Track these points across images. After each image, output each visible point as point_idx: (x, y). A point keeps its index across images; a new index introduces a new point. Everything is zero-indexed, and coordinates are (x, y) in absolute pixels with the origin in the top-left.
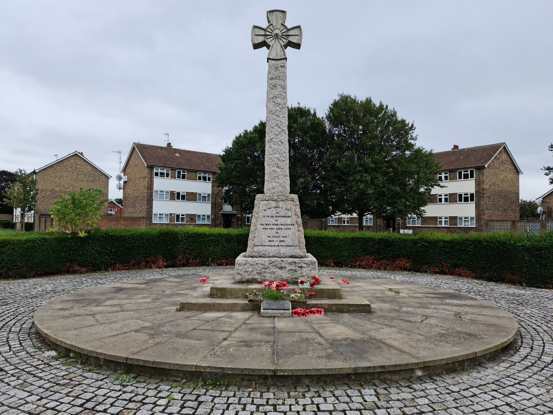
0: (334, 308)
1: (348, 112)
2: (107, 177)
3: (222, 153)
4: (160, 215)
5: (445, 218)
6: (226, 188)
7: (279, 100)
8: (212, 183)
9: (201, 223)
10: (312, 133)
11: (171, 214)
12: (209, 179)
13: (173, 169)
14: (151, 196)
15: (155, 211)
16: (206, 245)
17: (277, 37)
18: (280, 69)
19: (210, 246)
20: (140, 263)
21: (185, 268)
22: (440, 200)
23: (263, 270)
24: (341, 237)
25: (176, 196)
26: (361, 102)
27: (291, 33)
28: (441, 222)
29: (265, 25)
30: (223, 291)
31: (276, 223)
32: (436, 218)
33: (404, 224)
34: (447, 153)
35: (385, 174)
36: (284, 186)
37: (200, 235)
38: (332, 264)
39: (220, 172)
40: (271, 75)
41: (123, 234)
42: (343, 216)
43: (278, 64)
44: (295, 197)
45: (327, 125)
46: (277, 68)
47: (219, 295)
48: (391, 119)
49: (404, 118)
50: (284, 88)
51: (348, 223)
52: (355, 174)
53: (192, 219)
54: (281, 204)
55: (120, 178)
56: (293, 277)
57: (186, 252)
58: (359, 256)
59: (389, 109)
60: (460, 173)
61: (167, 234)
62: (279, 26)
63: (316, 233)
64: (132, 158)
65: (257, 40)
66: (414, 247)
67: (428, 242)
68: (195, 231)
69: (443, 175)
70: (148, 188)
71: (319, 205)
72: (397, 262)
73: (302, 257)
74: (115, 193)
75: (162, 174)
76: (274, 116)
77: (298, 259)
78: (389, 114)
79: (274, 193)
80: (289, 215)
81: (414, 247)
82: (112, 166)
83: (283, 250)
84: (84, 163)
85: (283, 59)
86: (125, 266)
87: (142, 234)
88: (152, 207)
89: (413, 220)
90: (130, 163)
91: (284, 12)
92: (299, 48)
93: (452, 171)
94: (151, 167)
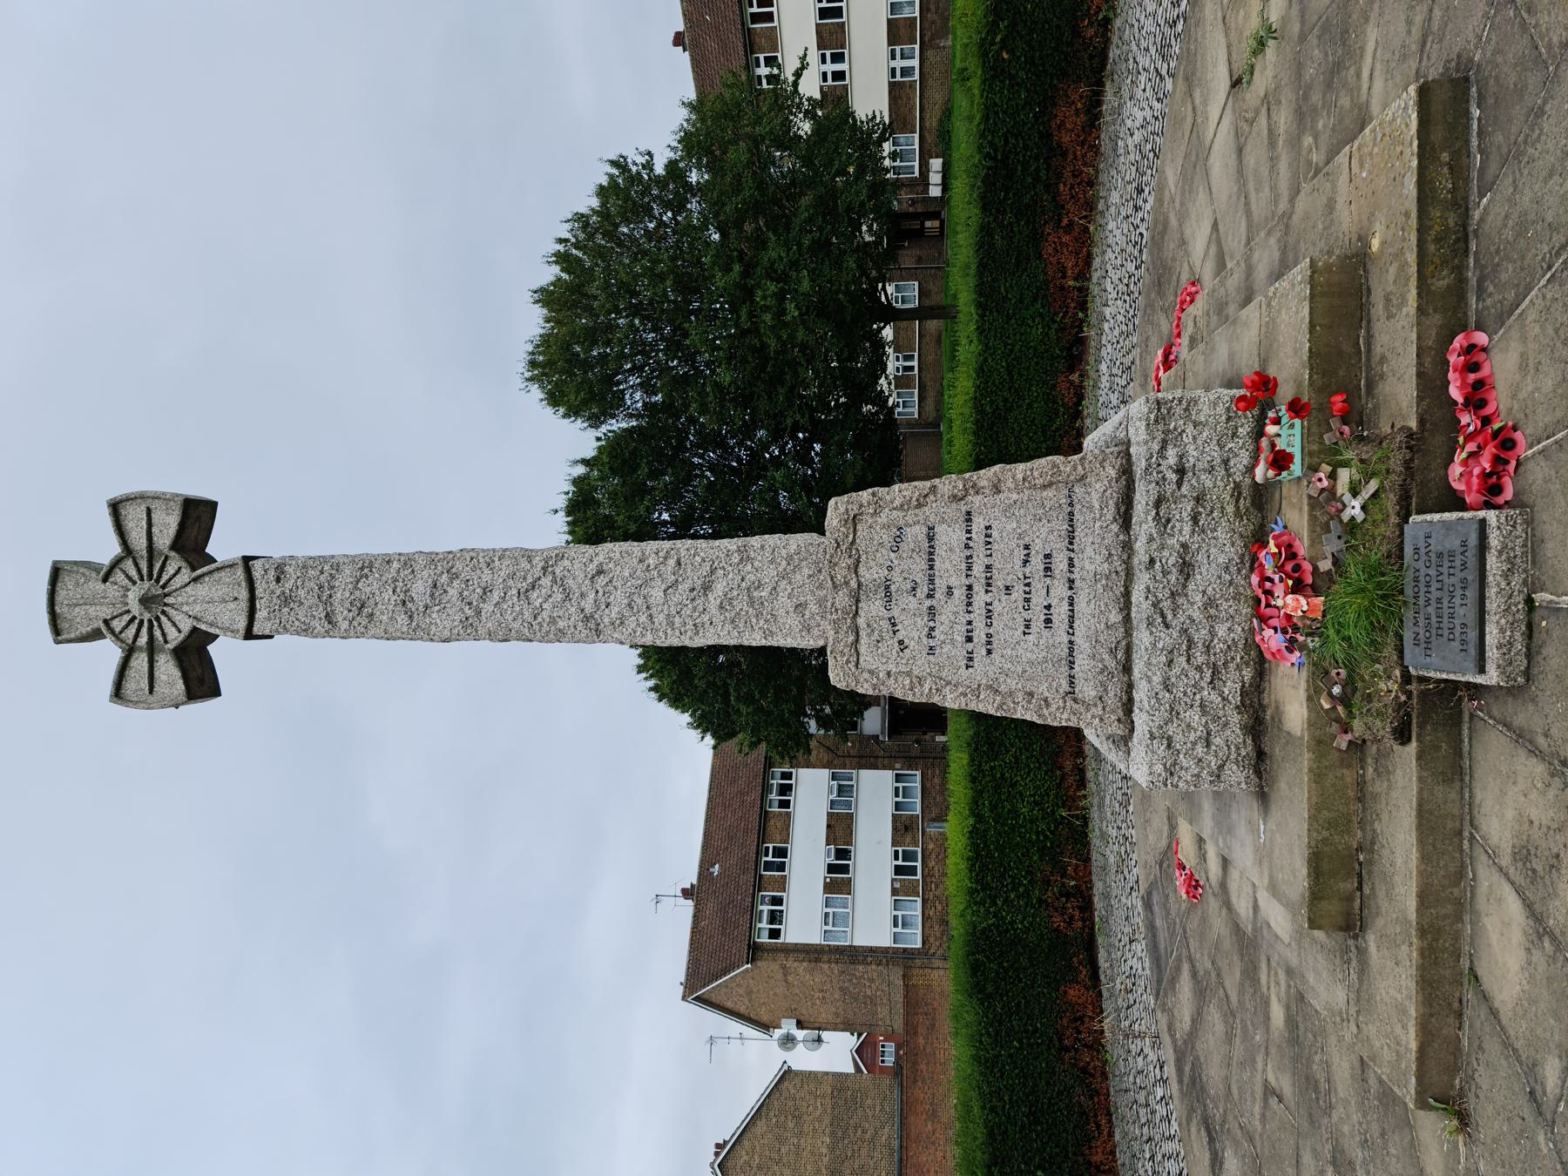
0: (1442, 282)
1: (573, 361)
2: (787, 1075)
3: (709, 740)
4: (896, 925)
5: (893, 58)
6: (813, 726)
7: (419, 588)
8: (798, 766)
9: (918, 801)
10: (644, 470)
11: (894, 892)
12: (787, 776)
13: (759, 884)
14: (839, 950)
15: (885, 941)
16: (1013, 828)
17: (165, 599)
18: (289, 585)
19: (1015, 813)
20: (1084, 1070)
21: (1098, 903)
22: (839, 76)
23: (1200, 658)
24: (975, 347)
25: (839, 878)
26: (548, 321)
27: (138, 541)
28: (906, 71)
29: (108, 653)
30: (1325, 865)
31: (959, 593)
32: (893, 86)
33: (912, 184)
34: (698, 66)
35: (760, 243)
36: (789, 559)
37: (975, 847)
38: (1075, 377)
39: (763, 745)
40: (315, 623)
41: (980, 1134)
42: (891, 366)
43: (285, 596)
44: (837, 508)
45: (616, 425)
46: (286, 600)
47: (1350, 885)
48: (597, 230)
49: (592, 189)
50: (366, 566)
51: (911, 358)
52: (759, 335)
53: (906, 828)
54: (871, 573)
55: (788, 1041)
56: (1230, 509)
57: (1040, 901)
58: (1046, 282)
59: (568, 236)
60: (756, 18)
61: (975, 968)
62: (112, 591)
63: (959, 439)
64: (729, 1005)
65: (171, 684)
66: (1012, 77)
67: (994, 24)
68: (963, 866)
69: (763, 71)
70: (817, 960)
71: (856, 446)
72: (1066, 139)
73: (1127, 471)
74: (835, 1053)
75: (775, 917)
76: (487, 608)
77: (1140, 487)
78: (582, 236)
79: (821, 602)
80: (922, 537)
81: (1012, 77)
82: (752, 1061)
83: (1092, 560)
84: (746, 1143)
85: (248, 571)
86: (1098, 1126)
87: (976, 1059)
88: (872, 950)
89: (901, 155)
90: (742, 1009)
91: (56, 572)
92: (212, 506)
93: (751, 45)
94: (755, 952)
